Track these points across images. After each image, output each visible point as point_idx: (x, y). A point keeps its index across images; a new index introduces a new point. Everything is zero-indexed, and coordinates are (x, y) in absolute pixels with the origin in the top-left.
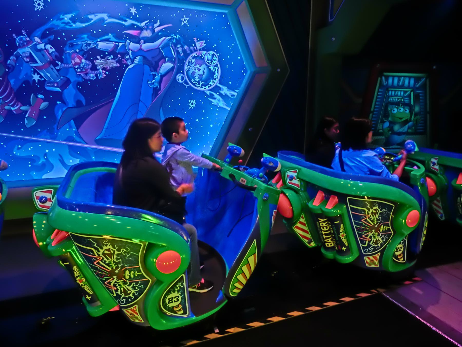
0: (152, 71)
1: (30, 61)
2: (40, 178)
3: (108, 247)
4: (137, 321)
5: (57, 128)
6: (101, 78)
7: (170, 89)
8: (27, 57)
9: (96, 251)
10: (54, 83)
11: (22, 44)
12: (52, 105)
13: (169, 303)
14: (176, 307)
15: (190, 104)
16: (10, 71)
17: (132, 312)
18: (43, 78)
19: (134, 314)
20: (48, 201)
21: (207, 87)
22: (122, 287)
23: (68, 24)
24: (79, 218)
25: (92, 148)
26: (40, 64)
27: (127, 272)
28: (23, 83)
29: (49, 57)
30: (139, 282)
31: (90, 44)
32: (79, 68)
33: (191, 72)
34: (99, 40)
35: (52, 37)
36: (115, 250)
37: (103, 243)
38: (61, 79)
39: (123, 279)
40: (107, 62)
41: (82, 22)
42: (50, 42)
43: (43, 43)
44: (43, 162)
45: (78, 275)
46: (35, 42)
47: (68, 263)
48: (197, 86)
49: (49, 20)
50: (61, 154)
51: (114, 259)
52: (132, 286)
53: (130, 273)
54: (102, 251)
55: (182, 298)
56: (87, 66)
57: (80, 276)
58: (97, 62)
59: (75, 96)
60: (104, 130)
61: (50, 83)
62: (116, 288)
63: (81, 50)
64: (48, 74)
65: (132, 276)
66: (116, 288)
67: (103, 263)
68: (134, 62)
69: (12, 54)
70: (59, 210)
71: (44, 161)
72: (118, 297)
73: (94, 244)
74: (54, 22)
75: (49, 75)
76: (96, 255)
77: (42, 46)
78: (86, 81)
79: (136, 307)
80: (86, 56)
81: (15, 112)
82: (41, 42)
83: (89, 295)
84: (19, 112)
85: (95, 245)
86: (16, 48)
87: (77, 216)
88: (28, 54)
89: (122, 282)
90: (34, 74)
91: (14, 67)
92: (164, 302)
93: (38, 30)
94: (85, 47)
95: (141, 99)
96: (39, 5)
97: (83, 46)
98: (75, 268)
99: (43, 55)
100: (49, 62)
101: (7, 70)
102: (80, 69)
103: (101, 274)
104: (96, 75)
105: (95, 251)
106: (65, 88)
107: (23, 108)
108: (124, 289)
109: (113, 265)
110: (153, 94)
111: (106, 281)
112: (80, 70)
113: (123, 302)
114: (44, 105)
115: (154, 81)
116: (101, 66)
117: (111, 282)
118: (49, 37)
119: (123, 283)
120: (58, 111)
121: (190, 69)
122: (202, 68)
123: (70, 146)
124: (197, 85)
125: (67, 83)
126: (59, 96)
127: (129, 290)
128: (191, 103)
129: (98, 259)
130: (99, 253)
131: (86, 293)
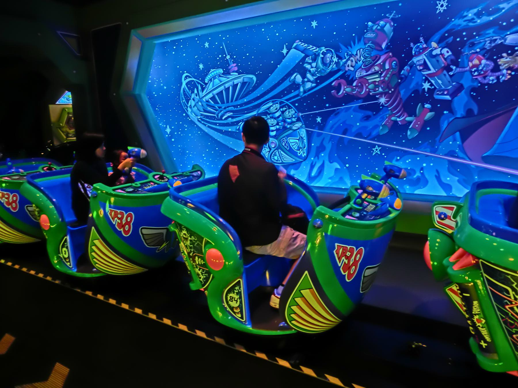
1: (423, 69)
6: (504, 81)
8: (420, 65)
9: (514, 293)
10: (444, 90)
11: (418, 52)
12: (438, 115)
16: (402, 81)
18: (434, 85)
20: (448, 219)
23: (471, 20)
24: (493, 244)
25: (477, 166)
26: (433, 71)
28: (412, 93)
29: (443, 62)
31: (496, 40)
32: (477, 70)
34: (508, 33)
35: (451, 39)
41: (490, 14)
42: (448, 46)
43: (439, 48)
44: (418, 176)
45: (477, 313)
46: (432, 47)
47: (468, 295)
49: (450, 21)
50: (439, 171)
56: (487, 67)
57: (479, 315)
58: (501, 61)
60: (495, 146)
61: (440, 91)
63: (482, 49)
69: (406, 64)
70: (469, 229)
71: (420, 175)
73: (513, 283)
74: (457, 22)
75: (440, 82)
76: (512, 298)
77: (437, 51)
78: (483, 85)
80: (487, 56)
81: (400, 123)
82: (438, 47)
83: (485, 341)
84: (405, 123)
85: (514, 285)
86: (412, 57)
88: (422, 62)
90: (425, 83)
91: (406, 77)
93: (436, 34)
94: (489, 45)
96: (442, 7)
97: (486, 44)
98: (475, 303)
99: (438, 61)
100: (443, 67)
101: (399, 81)
102: (478, 72)
103: (510, 322)
104: (498, 78)
106: (456, 96)
107: (408, 119)
112: (477, 73)
114: (429, 115)
116: (506, 65)
118: (447, 40)
120: (443, 124)
123: (449, 161)
125: (460, 88)
126: (447, 105)
129: (514, 303)
131: (479, 337)
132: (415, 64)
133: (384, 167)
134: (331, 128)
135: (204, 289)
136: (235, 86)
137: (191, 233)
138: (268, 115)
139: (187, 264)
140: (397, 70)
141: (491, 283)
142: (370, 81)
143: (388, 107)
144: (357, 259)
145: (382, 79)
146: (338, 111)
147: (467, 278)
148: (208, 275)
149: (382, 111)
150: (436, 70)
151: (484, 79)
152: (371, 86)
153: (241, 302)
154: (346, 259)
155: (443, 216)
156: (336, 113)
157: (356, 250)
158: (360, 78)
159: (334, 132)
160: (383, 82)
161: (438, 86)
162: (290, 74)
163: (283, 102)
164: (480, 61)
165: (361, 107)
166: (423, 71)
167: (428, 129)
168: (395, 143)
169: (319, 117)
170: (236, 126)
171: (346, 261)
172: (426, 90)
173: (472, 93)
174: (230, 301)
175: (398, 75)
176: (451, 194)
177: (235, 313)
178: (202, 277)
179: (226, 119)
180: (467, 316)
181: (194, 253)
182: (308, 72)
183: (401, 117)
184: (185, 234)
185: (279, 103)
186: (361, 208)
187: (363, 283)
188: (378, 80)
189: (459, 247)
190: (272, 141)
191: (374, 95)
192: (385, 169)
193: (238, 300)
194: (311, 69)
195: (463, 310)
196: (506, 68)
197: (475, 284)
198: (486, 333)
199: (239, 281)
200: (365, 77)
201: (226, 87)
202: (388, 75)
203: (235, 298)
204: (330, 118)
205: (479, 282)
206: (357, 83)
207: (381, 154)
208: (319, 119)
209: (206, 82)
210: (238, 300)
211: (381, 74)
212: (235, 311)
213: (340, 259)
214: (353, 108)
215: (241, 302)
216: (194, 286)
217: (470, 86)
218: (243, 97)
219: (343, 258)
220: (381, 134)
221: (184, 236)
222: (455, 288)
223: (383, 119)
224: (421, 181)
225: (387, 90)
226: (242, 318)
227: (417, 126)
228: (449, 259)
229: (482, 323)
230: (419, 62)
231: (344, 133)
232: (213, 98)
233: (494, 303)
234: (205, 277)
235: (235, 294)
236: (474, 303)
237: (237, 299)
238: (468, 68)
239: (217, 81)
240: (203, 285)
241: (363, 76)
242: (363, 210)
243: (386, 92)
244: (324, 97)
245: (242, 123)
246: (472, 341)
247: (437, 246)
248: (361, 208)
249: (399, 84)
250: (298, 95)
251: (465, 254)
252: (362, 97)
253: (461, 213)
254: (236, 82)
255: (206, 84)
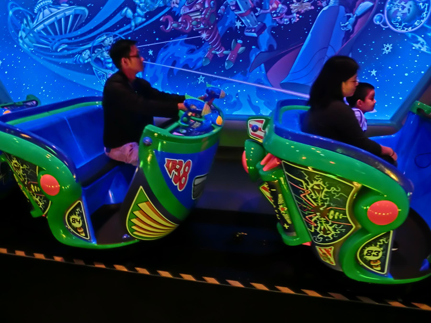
0: (347, 13)
1: (235, 9)
2: (231, 114)
3: (318, 183)
4: (328, 262)
5: (250, 71)
6: (294, 22)
7: (364, 31)
9: (306, 184)
10: (252, 29)
12: (248, 50)
13: (367, 255)
14: (374, 261)
15: (385, 49)
17: (326, 252)
19: (328, 255)
21: (410, 28)
22: (323, 225)
26: (243, 11)
27: (332, 212)
30: (341, 225)
33: (394, 10)
36: (325, 187)
37: (315, 177)
38: (258, 25)
39: (325, 218)
40: (302, 5)
44: (234, 101)
47: (274, 190)
48: (398, 28)
51: (321, 196)
52: (333, 227)
53: (335, 213)
54: (311, 185)
55: (383, 255)
59: (269, 40)
61: (249, 29)
62: (316, 225)
64: (247, 21)
65: (336, 218)
66: (316, 225)
67: (310, 197)
68: (330, 3)
70: (275, 137)
72: (316, 233)
73: (305, 176)
75: (248, 21)
76: (305, 188)
78: (280, 25)
79: (331, 249)
81: (219, 56)
84: (223, 56)
85: (306, 178)
87: (289, 146)
88: (234, 3)
89: (324, 220)
90: (237, 21)
91: (222, 15)
92: (362, 252)
95: (331, 44)
98: (280, 195)
104: (290, 20)
105: (305, 184)
106: (261, 34)
107: (225, 52)
108: (324, 228)
109: (319, 202)
110: (344, 38)
111: (307, 215)
113: (319, 240)
114: (241, 49)
115: (347, 23)
116: (296, 10)
117: (313, 218)
119: (325, 222)
120: (252, 56)
121: (393, 8)
122: (407, 6)
123: (258, 88)
124: (397, 26)
125: (263, 28)
126: (255, 41)
127: (329, 231)
128: (386, 48)
129: (306, 192)
130: (308, 187)
131: (284, 221)
132: (229, 4)
133: (206, 89)
134: (163, 59)
135: (45, 215)
136: (67, 18)
137: (22, 162)
138: (103, 48)
139: (25, 193)
140: (214, 10)
141: (291, 179)
142: (193, 18)
143: (209, 41)
144: (186, 171)
145: (203, 16)
146: (167, 45)
147: (273, 176)
148: (46, 201)
149: (205, 45)
150: (246, 11)
151: (280, 20)
152: (194, 23)
153: (84, 222)
154: (176, 172)
155: (256, 129)
156: (166, 47)
157: (185, 162)
158: (185, 15)
159: (164, 64)
160: (204, 19)
161: (247, 25)
162: (120, 9)
163: (117, 36)
164: (278, 6)
165: (186, 41)
166: (235, 11)
167: (241, 61)
168: (215, 73)
169: (150, 50)
170: (72, 59)
171: (177, 173)
172: (238, 27)
173: (272, 32)
174: (72, 222)
175: (216, 13)
176: (259, 114)
177: (79, 233)
178: (41, 204)
179: (61, 51)
180: (275, 206)
181: (28, 181)
182: (137, 7)
183: (219, 51)
184: (16, 163)
185: (112, 36)
186: (187, 125)
187: (194, 191)
188: (199, 17)
189: (268, 153)
190: (109, 73)
191: (197, 31)
192: (207, 91)
193: (81, 221)
194: (141, 5)
195: (272, 202)
196: (296, 12)
197: (280, 181)
198: (288, 218)
199: (79, 204)
200: (188, 14)
201: (58, 18)
202: (208, 14)
203: (77, 219)
204: (160, 51)
205: (282, 179)
206: (182, 20)
207: (205, 82)
208: (151, 52)
209: (36, 12)
210: (81, 221)
211: (202, 12)
212: (79, 231)
213: (170, 172)
214: (180, 42)
215: (84, 222)
216: (35, 214)
217: (270, 26)
218: (76, 30)
219: (174, 171)
220: (204, 65)
221: (15, 165)
222: (266, 186)
223: (205, 52)
224: (237, 105)
225: (207, 27)
226: (86, 236)
227: (232, 58)
228: (260, 163)
229: (285, 210)
230: (233, 3)
231: (173, 65)
232: (45, 29)
233: (293, 194)
234: (43, 203)
235: (77, 215)
236: (279, 196)
237: (80, 220)
238: (269, 11)
239: (47, 11)
240: (44, 211)
241: (186, 13)
242: (190, 127)
243: (206, 28)
244: (154, 31)
245: (78, 56)
246: (279, 225)
247: (252, 151)
248: (187, 125)
249: (217, 22)
250: (130, 29)
251: (272, 157)
252: (187, 32)
253: (269, 125)
254: (67, 13)
255: (36, 14)
